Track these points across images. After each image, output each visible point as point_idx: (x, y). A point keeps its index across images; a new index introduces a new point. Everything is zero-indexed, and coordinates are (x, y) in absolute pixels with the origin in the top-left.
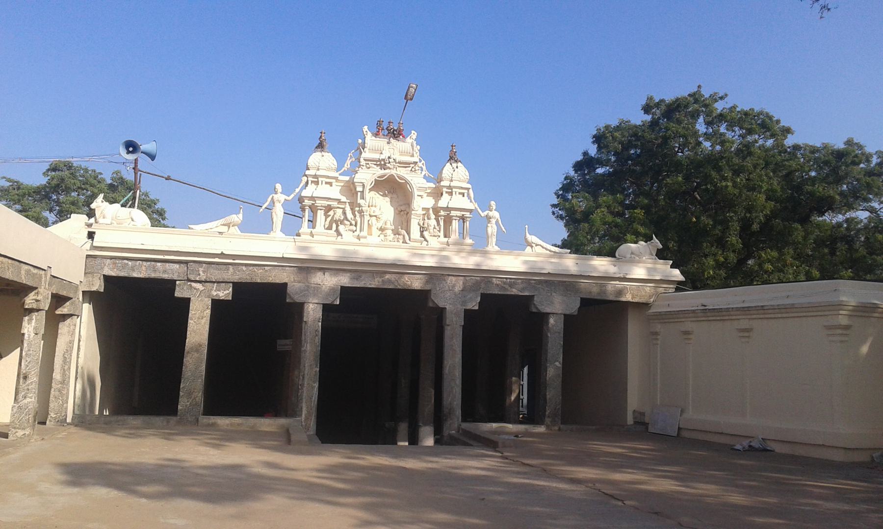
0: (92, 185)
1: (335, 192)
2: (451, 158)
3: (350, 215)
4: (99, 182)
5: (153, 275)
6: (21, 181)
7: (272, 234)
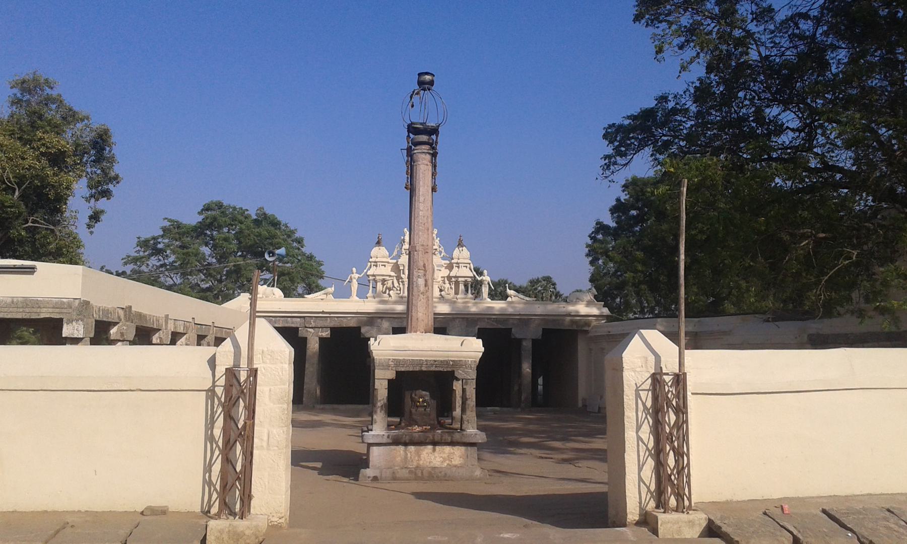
0: (241, 223)
1: (387, 270)
3: (396, 284)
4: (246, 218)
5: (286, 325)
6: (180, 220)
7: (351, 299)
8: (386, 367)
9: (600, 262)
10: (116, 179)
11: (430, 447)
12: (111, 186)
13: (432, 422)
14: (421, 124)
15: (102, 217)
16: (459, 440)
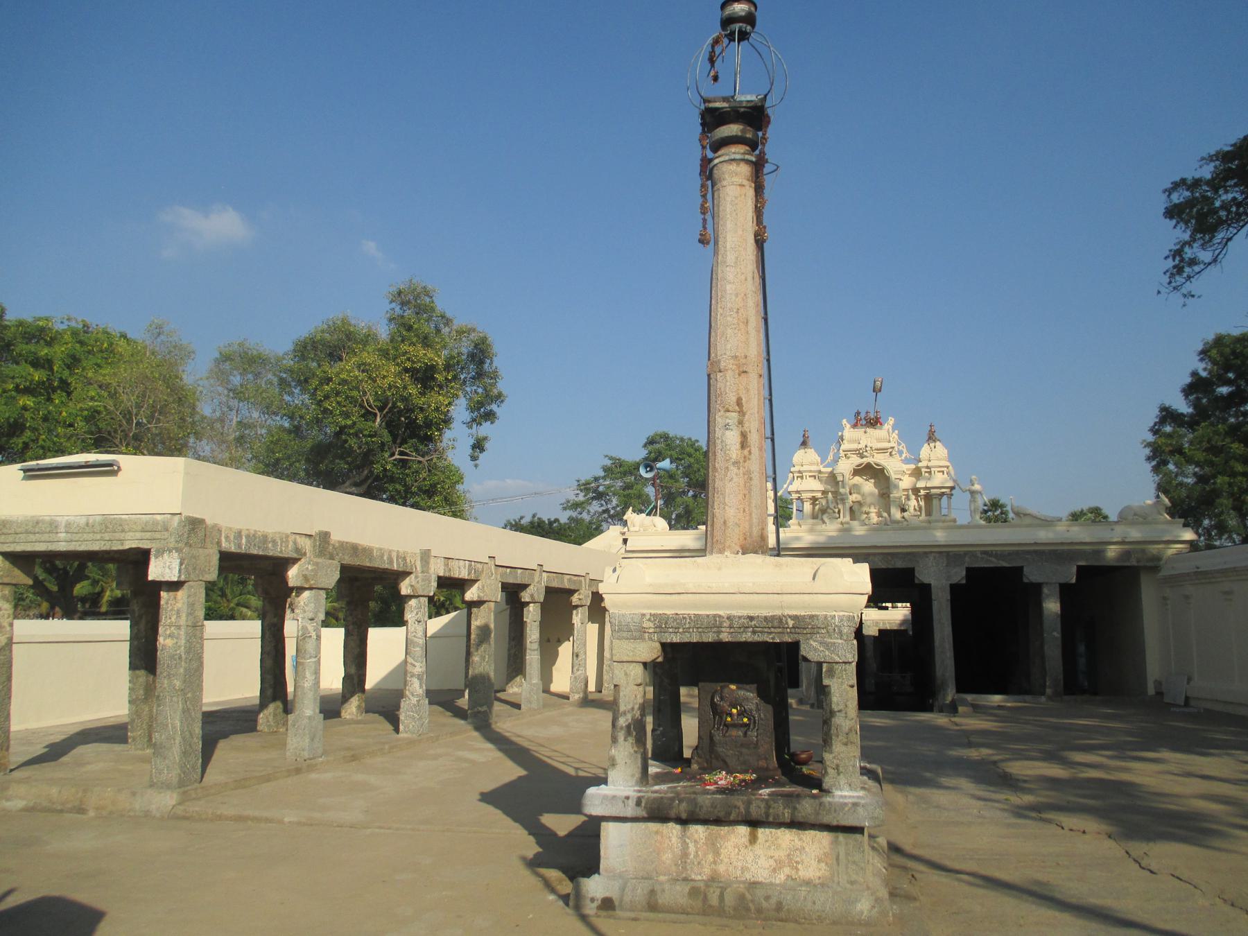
0: (690, 455)
2: (930, 438)
8: (637, 633)
9: (1171, 467)
10: (499, 398)
11: (743, 830)
12: (494, 407)
13: (762, 763)
14: (725, 99)
15: (487, 445)
16: (812, 819)
